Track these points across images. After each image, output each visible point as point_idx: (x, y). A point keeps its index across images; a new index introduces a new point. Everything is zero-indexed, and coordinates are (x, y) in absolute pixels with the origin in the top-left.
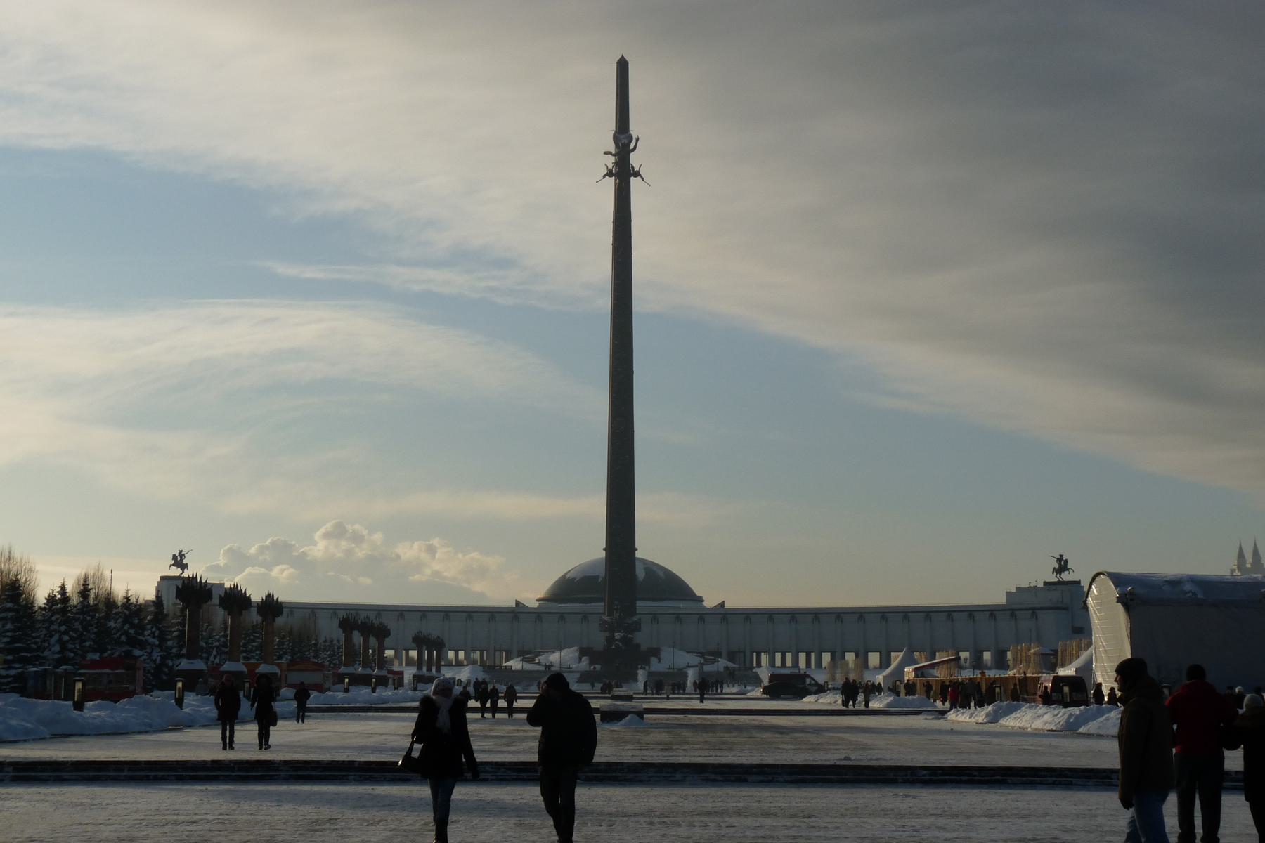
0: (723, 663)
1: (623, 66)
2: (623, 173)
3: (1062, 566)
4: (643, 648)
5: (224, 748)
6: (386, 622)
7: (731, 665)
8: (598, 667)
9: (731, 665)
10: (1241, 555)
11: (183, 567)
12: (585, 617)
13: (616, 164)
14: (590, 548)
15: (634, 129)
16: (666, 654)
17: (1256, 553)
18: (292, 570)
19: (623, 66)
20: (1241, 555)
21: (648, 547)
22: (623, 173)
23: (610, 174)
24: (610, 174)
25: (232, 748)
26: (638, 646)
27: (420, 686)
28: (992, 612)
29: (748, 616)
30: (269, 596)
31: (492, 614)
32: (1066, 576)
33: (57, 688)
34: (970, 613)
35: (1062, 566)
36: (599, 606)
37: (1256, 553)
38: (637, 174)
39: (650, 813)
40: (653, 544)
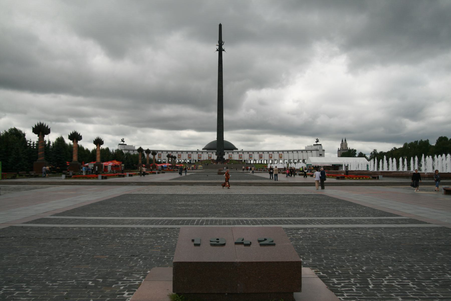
1: (220, 26)
19: (220, 26)
23: (217, 50)
24: (217, 50)
38: (224, 50)
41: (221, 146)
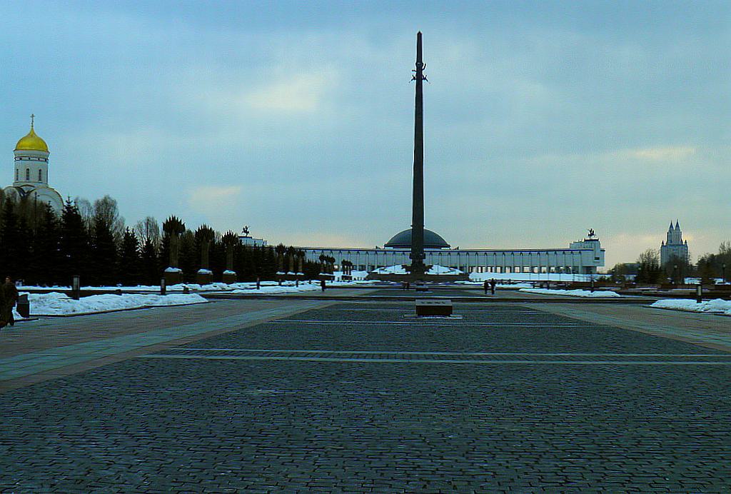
0: (458, 272)
1: (419, 35)
3: (592, 234)
4: (426, 265)
5: (511, 272)
6: (334, 257)
7: (461, 272)
8: (409, 273)
9: (461, 272)
10: (671, 226)
13: (417, 75)
14: (407, 224)
16: (435, 267)
17: (677, 225)
18: (425, 250)
19: (419, 35)
20: (671, 226)
21: (427, 226)
23: (414, 78)
24: (414, 78)
25: (514, 272)
26: (424, 265)
32: (593, 238)
33: (491, 269)
37: (677, 225)
38: (425, 79)
39: (510, 284)
41: (418, 241)
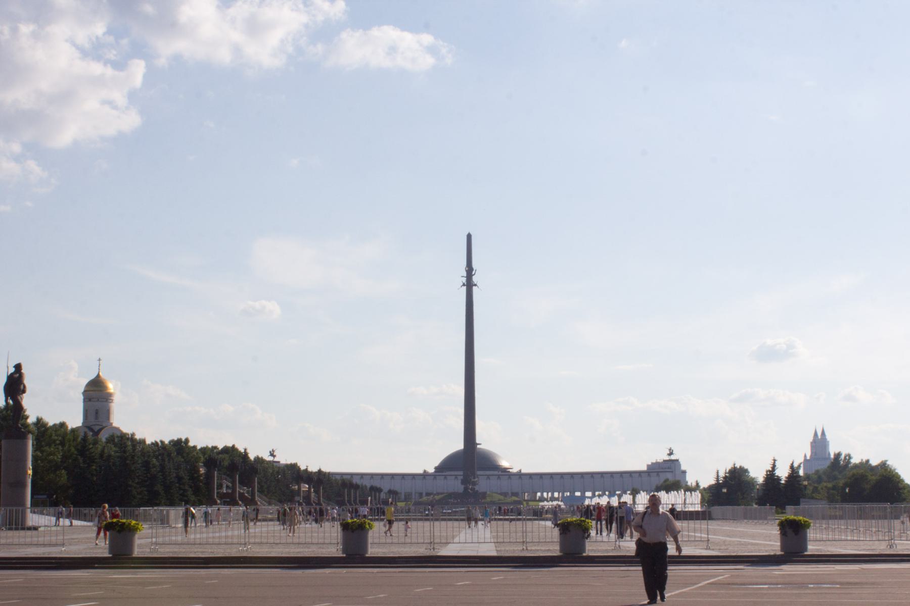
1: (469, 237)
2: (469, 285)
11: (274, 456)
12: (456, 476)
15: (475, 265)
17: (823, 433)
19: (469, 237)
22: (469, 285)
23: (464, 285)
24: (464, 285)
27: (597, 511)
28: (640, 473)
29: (531, 476)
30: (233, 446)
31: (414, 476)
32: (673, 457)
34: (631, 474)
35: (671, 454)
36: (461, 473)
40: (485, 440)
